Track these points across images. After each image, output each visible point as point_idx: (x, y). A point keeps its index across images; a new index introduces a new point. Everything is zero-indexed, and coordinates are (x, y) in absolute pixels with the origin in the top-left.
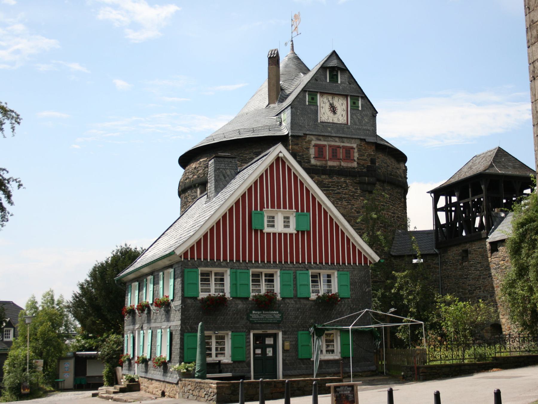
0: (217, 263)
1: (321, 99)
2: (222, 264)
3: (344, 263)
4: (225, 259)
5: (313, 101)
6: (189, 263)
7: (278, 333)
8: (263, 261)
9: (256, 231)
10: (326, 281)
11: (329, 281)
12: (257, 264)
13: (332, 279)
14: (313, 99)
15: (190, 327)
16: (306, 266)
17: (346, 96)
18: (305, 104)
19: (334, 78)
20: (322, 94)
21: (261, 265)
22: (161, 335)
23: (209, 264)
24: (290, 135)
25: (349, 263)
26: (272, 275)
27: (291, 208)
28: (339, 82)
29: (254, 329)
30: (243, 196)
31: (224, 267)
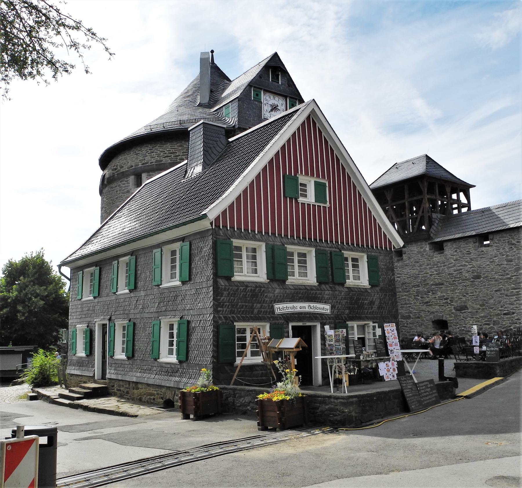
0: (251, 235)
1: (265, 97)
2: (257, 236)
3: (372, 246)
4: (260, 232)
5: (257, 97)
6: (221, 232)
7: (315, 326)
8: (298, 237)
9: (291, 199)
10: (250, 257)
11: (254, 257)
12: (293, 240)
13: (258, 254)
14: (257, 95)
15: (224, 317)
16: (340, 247)
17: (285, 97)
18: (251, 100)
19: (276, 78)
20: (266, 91)
21: (296, 241)
22: (83, 277)
23: (242, 235)
24: (237, 127)
25: (377, 247)
26: (304, 255)
27: (323, 177)
28: (280, 83)
29: (292, 321)
30: (277, 154)
31: (259, 240)
